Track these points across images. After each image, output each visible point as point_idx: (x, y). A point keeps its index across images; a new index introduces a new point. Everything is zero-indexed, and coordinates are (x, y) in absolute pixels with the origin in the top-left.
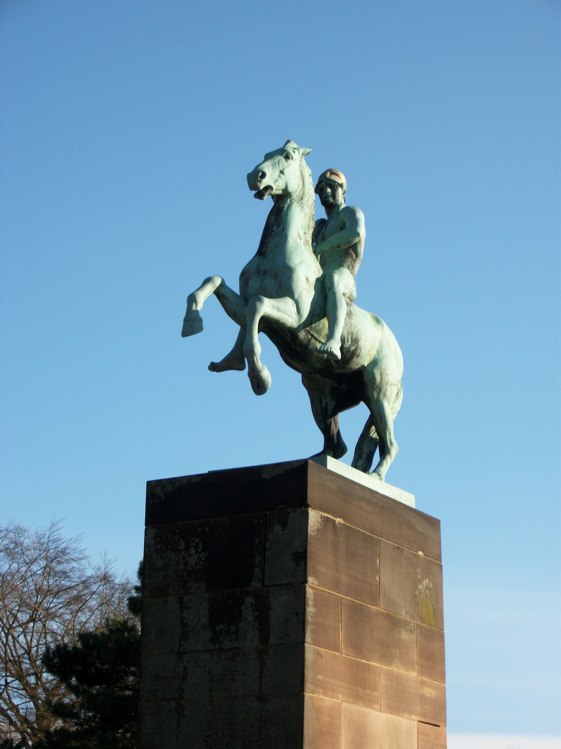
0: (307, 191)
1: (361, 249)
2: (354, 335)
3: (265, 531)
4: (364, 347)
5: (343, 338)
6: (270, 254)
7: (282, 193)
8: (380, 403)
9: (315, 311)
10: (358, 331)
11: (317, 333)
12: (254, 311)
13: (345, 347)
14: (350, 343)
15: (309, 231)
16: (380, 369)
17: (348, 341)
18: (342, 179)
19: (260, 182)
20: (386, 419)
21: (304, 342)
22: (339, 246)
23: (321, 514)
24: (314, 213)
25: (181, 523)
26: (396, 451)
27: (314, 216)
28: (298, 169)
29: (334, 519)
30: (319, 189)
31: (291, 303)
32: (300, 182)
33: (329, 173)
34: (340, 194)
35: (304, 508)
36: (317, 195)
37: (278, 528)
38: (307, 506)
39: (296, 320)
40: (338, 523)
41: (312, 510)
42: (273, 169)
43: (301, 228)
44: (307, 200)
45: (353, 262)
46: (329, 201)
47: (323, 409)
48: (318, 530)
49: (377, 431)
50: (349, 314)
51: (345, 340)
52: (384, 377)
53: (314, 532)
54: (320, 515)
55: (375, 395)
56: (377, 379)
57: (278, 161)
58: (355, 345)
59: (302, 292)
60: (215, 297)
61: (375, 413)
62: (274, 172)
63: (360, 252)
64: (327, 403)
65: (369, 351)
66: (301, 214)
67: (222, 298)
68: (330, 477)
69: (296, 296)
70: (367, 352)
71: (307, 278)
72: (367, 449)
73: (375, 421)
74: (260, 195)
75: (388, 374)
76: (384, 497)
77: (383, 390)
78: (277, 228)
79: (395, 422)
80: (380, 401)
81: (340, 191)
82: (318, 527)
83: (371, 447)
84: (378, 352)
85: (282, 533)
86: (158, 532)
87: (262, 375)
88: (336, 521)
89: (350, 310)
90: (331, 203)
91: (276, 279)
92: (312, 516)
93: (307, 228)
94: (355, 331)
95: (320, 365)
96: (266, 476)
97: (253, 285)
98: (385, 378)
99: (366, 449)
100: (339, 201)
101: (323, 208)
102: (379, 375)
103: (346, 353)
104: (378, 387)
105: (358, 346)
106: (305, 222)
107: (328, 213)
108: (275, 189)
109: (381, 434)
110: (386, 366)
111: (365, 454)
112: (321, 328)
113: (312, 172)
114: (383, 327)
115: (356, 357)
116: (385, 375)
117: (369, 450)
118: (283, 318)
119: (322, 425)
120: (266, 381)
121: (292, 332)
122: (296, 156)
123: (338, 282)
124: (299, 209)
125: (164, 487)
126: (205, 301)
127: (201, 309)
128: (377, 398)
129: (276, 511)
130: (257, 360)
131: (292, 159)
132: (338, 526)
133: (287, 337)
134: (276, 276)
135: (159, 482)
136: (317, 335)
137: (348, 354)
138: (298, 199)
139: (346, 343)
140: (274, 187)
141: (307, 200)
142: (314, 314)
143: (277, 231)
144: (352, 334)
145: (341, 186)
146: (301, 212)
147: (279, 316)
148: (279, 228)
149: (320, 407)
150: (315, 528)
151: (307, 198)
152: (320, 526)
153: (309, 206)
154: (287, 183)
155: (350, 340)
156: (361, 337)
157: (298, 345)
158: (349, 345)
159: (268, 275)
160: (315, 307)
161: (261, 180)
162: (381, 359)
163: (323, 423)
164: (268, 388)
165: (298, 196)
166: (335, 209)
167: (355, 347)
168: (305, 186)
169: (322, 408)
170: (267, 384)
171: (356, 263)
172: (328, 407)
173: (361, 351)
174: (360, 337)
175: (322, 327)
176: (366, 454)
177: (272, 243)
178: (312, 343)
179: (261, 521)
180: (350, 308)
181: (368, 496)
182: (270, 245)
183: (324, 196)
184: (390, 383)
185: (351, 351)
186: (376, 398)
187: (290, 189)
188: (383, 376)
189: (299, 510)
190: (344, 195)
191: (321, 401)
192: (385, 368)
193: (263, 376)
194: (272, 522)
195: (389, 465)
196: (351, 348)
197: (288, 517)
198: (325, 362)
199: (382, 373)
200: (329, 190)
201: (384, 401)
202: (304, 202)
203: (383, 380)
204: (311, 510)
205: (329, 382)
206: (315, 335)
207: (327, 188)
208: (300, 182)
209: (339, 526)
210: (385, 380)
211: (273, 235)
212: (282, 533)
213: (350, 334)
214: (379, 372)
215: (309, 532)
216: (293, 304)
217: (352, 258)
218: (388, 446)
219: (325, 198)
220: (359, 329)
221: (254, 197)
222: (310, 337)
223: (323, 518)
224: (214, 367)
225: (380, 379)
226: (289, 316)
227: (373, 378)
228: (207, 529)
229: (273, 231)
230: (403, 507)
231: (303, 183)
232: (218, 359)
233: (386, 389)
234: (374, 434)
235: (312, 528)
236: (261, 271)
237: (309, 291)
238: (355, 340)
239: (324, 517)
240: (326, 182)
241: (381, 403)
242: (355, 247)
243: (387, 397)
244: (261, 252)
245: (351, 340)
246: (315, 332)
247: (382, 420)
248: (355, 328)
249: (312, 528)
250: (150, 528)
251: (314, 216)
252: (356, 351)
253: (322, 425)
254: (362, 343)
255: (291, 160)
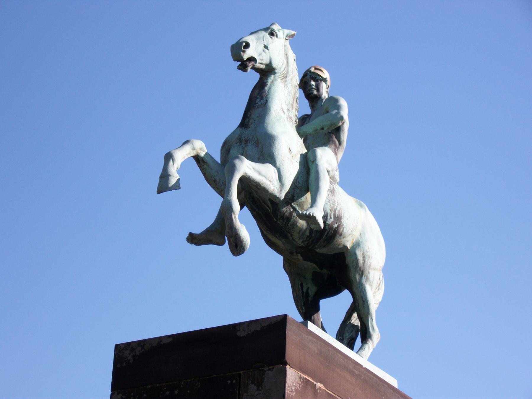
0: (291, 71)
1: (344, 138)
2: (337, 212)
3: (239, 392)
4: (347, 226)
5: (325, 213)
6: (253, 124)
7: (265, 68)
8: (362, 286)
9: (298, 183)
10: (341, 209)
11: (299, 206)
12: (233, 169)
13: (327, 224)
14: (332, 220)
15: (293, 109)
16: (362, 251)
17: (331, 218)
18: (325, 74)
19: (244, 52)
20: (369, 302)
21: (286, 214)
22: (322, 129)
23: (300, 375)
24: (298, 96)
25: (149, 387)
26: (378, 339)
27: (298, 99)
28: (283, 48)
29: (315, 383)
30: (304, 84)
31: (273, 170)
32: (284, 60)
33: (313, 68)
34: (324, 88)
35: (281, 366)
36: (301, 90)
37: (252, 388)
38: (285, 363)
39: (278, 188)
40: (318, 388)
41: (290, 368)
42: (257, 43)
43: (285, 104)
44: (291, 79)
45: (336, 149)
46: (312, 93)
47: (304, 293)
48: (296, 390)
49: (360, 318)
50: (332, 191)
51: (327, 216)
52: (366, 259)
53: (292, 392)
54: (299, 375)
55: (358, 277)
56: (359, 261)
57: (262, 37)
58: (338, 222)
59: (284, 160)
60: (194, 162)
61: (357, 296)
62: (258, 45)
63: (343, 141)
64: (308, 288)
65: (352, 231)
66: (285, 90)
67: (202, 163)
68: (310, 338)
69: (278, 164)
70: (350, 231)
71: (289, 148)
72: (348, 335)
73: (357, 305)
74: (243, 66)
75: (371, 257)
76: (367, 371)
77: (366, 272)
78: (260, 101)
79: (377, 311)
80: (362, 284)
81: (323, 85)
82: (297, 388)
83: (353, 333)
84: (360, 234)
85: (257, 393)
86: (124, 397)
87: (240, 233)
88: (316, 385)
89: (333, 188)
90: (315, 95)
91: (257, 147)
92: (291, 374)
93: (290, 106)
94: (338, 209)
95: (302, 242)
96: (241, 333)
97: (234, 153)
98: (368, 261)
99: (347, 334)
100: (322, 95)
101: (307, 102)
102: (362, 257)
103: (329, 230)
104: (360, 270)
105: (341, 224)
106: (288, 99)
107: (312, 106)
108: (259, 63)
109: (363, 319)
110: (369, 248)
111: (347, 339)
112: (304, 202)
113: (296, 57)
114: (366, 211)
115: (338, 236)
116: (368, 258)
117: (350, 335)
118: (264, 183)
119: (302, 310)
120: (244, 240)
121: (273, 200)
122: (282, 33)
123: (321, 156)
124: (283, 86)
125: (132, 350)
126: (183, 162)
127: (179, 168)
128: (359, 281)
129: (251, 370)
130: (235, 217)
131: (277, 37)
132: (318, 391)
133: (269, 209)
134: (257, 144)
135: (128, 345)
136: (299, 208)
137: (331, 231)
138: (282, 77)
139: (328, 219)
140: (258, 60)
141: (291, 79)
142: (296, 186)
143: (260, 103)
144: (335, 211)
145: (325, 80)
146: (285, 89)
147: (260, 180)
148: (262, 100)
149: (301, 291)
150: (293, 388)
151: (291, 77)
152: (298, 387)
153: (293, 86)
154: (271, 58)
155: (332, 217)
156: (343, 215)
157: (279, 217)
158: (332, 222)
159: (249, 143)
160: (297, 179)
161: (245, 50)
162: (364, 241)
163: (304, 308)
164: (247, 248)
165: (282, 73)
166: (319, 102)
167: (337, 224)
168: (289, 65)
169: (303, 292)
170: (245, 244)
171: (339, 150)
172: (310, 292)
173: (343, 229)
174: (342, 215)
175: (304, 200)
176: (347, 340)
177: (255, 114)
178: (294, 216)
179: (234, 381)
180: (333, 186)
181: (351, 367)
182: (253, 116)
183: (308, 88)
184: (372, 267)
185: (334, 228)
186: (358, 281)
187: (274, 65)
188: (365, 258)
189: (276, 367)
190: (328, 90)
191: (302, 285)
192: (368, 251)
193: (241, 235)
194: (247, 382)
195: (371, 351)
196: (334, 225)
197: (264, 376)
198: (307, 238)
199: (365, 255)
200: (313, 83)
201: (366, 284)
202: (288, 80)
203: (366, 263)
204: (289, 368)
205: (310, 266)
206: (297, 208)
207: (310, 81)
208: (284, 60)
209: (320, 391)
210: (367, 263)
211: (256, 107)
212: (257, 393)
213: (333, 211)
214: (362, 254)
215: (287, 391)
216: (274, 170)
217: (335, 145)
218: (369, 332)
219: (309, 90)
220: (342, 207)
221: (237, 68)
222: (292, 210)
223: (303, 379)
224: (193, 239)
225: (363, 262)
226: (270, 181)
227: (356, 260)
228: (176, 392)
229: (256, 103)
230: (386, 386)
231: (288, 62)
232: (198, 230)
233: (369, 273)
234: (355, 320)
235: (290, 387)
236: (243, 140)
237: (292, 162)
238: (338, 217)
239: (304, 378)
240: (310, 76)
241: (363, 286)
242: (337, 131)
243: (370, 281)
244: (244, 124)
245: (334, 217)
246: (297, 205)
247: (364, 304)
248: (338, 205)
249: (290, 387)
250: (116, 393)
251: (298, 99)
252: (339, 228)
253: (302, 310)
254: (344, 221)
255: (276, 37)
